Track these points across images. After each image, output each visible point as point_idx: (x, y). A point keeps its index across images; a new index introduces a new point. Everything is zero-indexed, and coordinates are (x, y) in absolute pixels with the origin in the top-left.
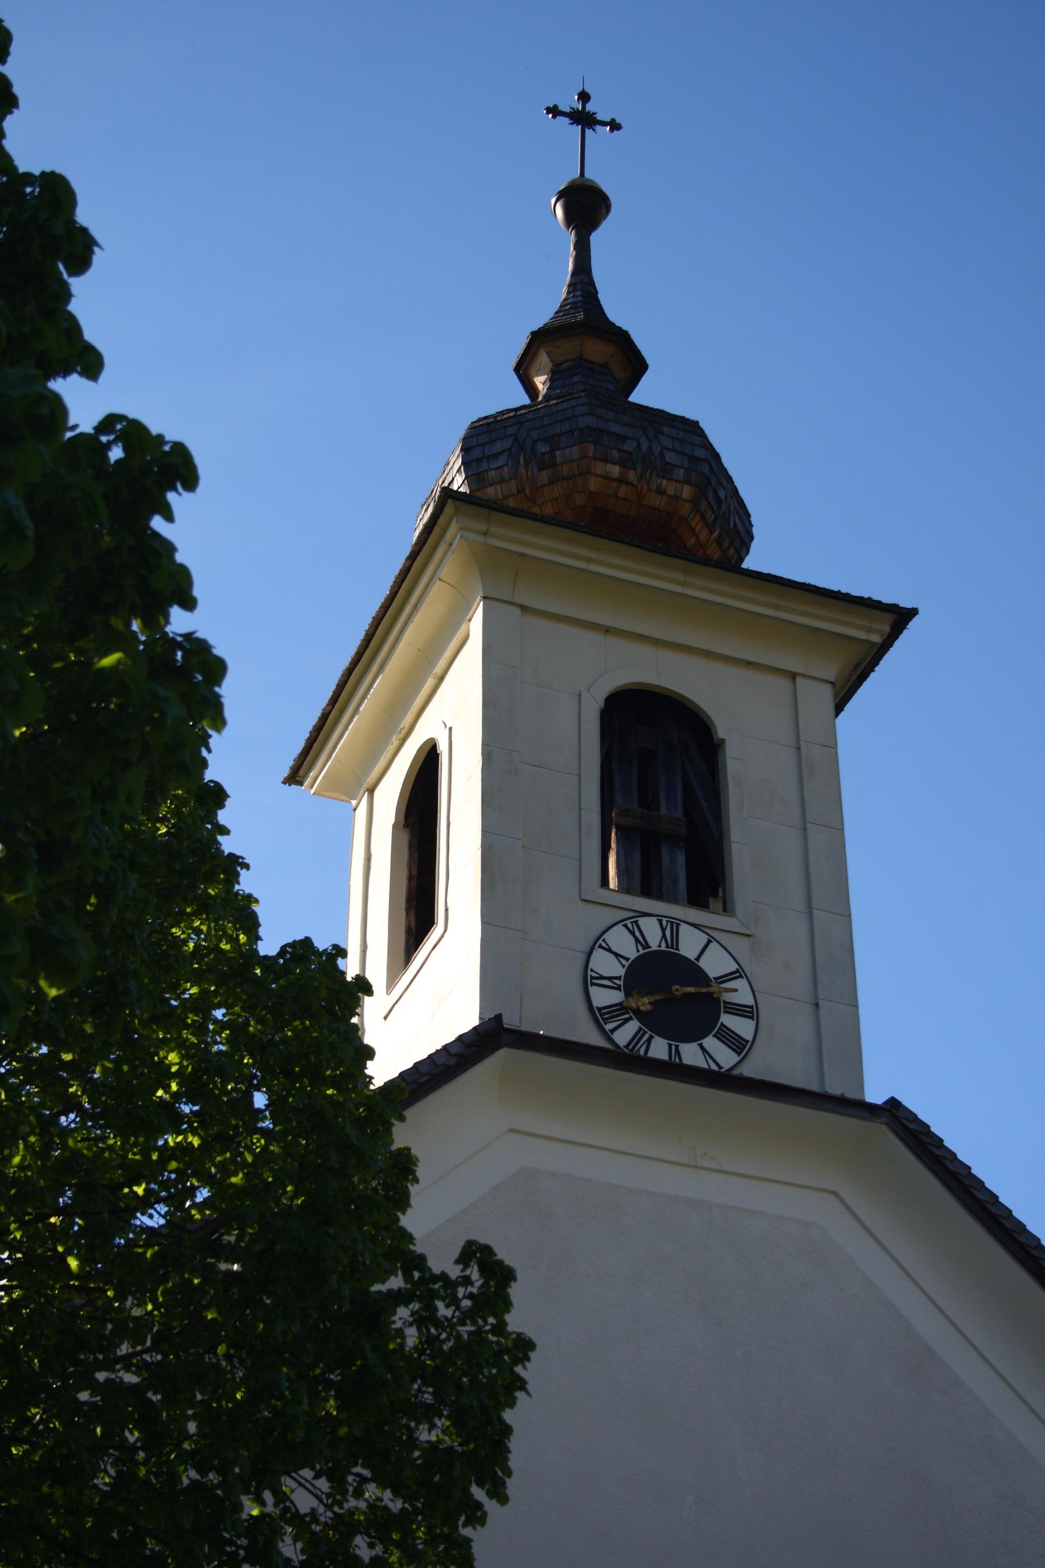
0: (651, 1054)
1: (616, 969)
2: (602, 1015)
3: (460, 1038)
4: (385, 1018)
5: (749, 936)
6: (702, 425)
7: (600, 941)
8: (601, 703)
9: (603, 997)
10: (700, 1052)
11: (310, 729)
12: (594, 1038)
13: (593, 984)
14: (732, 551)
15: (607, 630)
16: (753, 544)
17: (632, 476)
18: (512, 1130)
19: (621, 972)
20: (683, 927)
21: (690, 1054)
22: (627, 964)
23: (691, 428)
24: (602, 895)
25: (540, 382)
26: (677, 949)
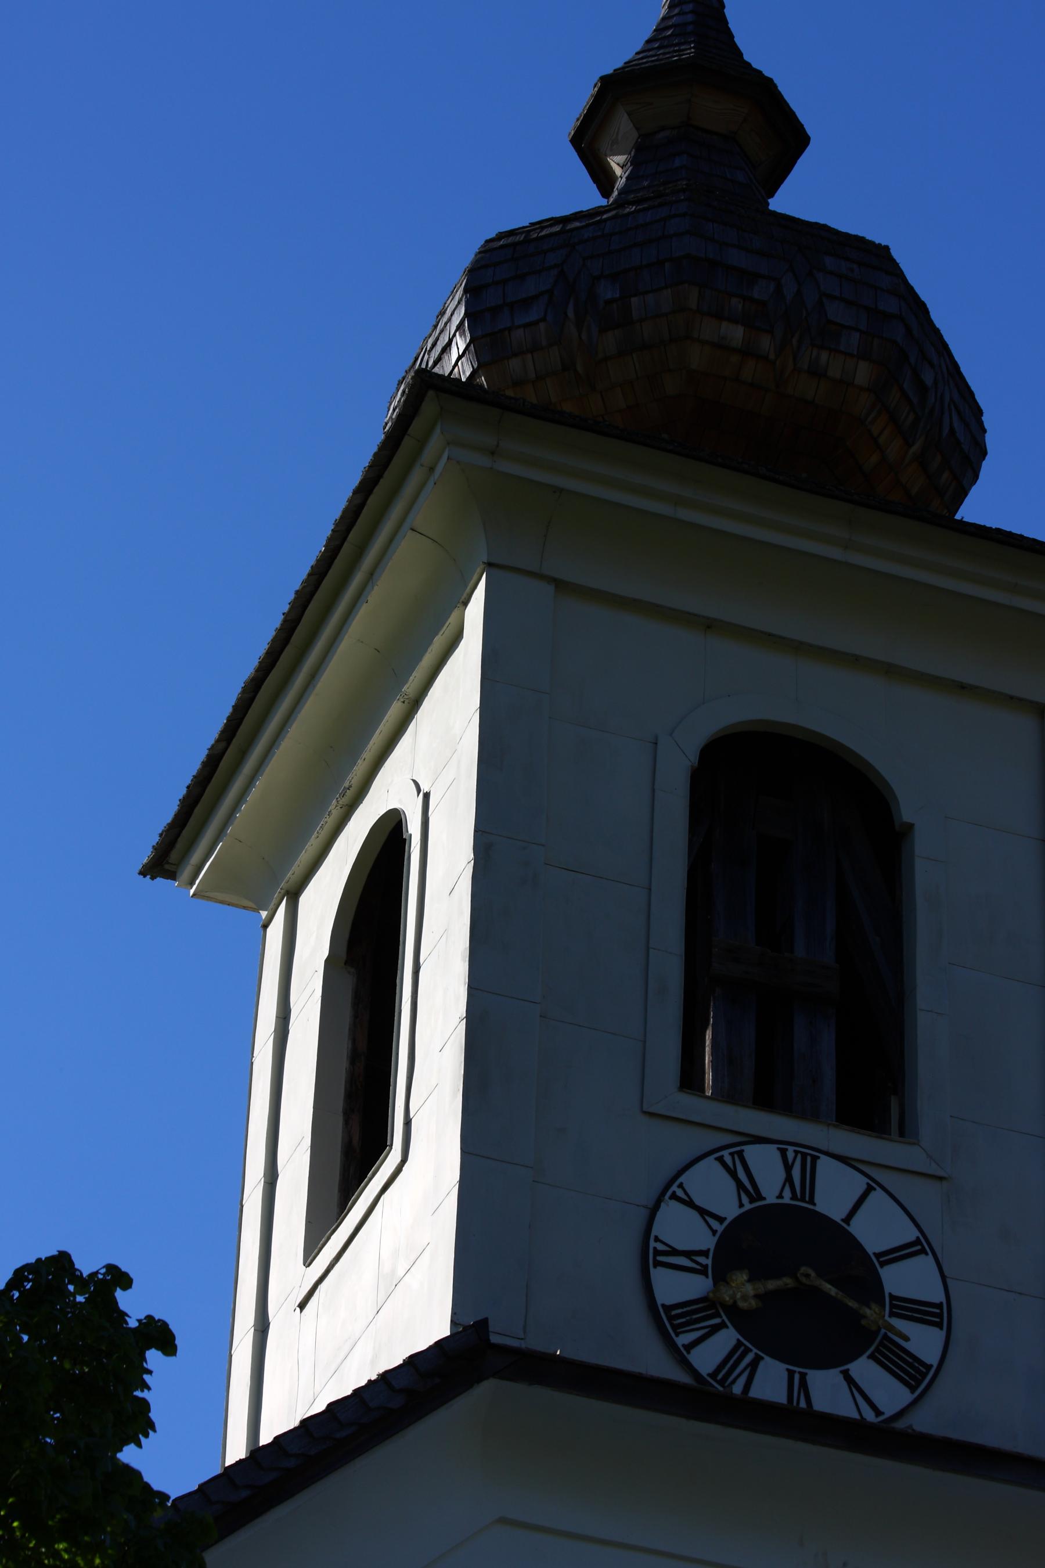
0: (755, 1393)
1: (699, 1237)
2: (671, 1319)
3: (413, 1360)
4: (302, 1306)
5: (941, 1179)
6: (895, 253)
7: (674, 1188)
8: (693, 757)
9: (675, 1287)
10: (844, 1384)
11: (188, 781)
12: (657, 1364)
13: (657, 1264)
14: (946, 475)
15: (710, 625)
16: (985, 464)
17: (766, 343)
18: (503, 1521)
19: (708, 1242)
20: (825, 1165)
21: (828, 1393)
22: (720, 1228)
23: (874, 260)
24: (686, 1103)
25: (617, 164)
26: (812, 1201)
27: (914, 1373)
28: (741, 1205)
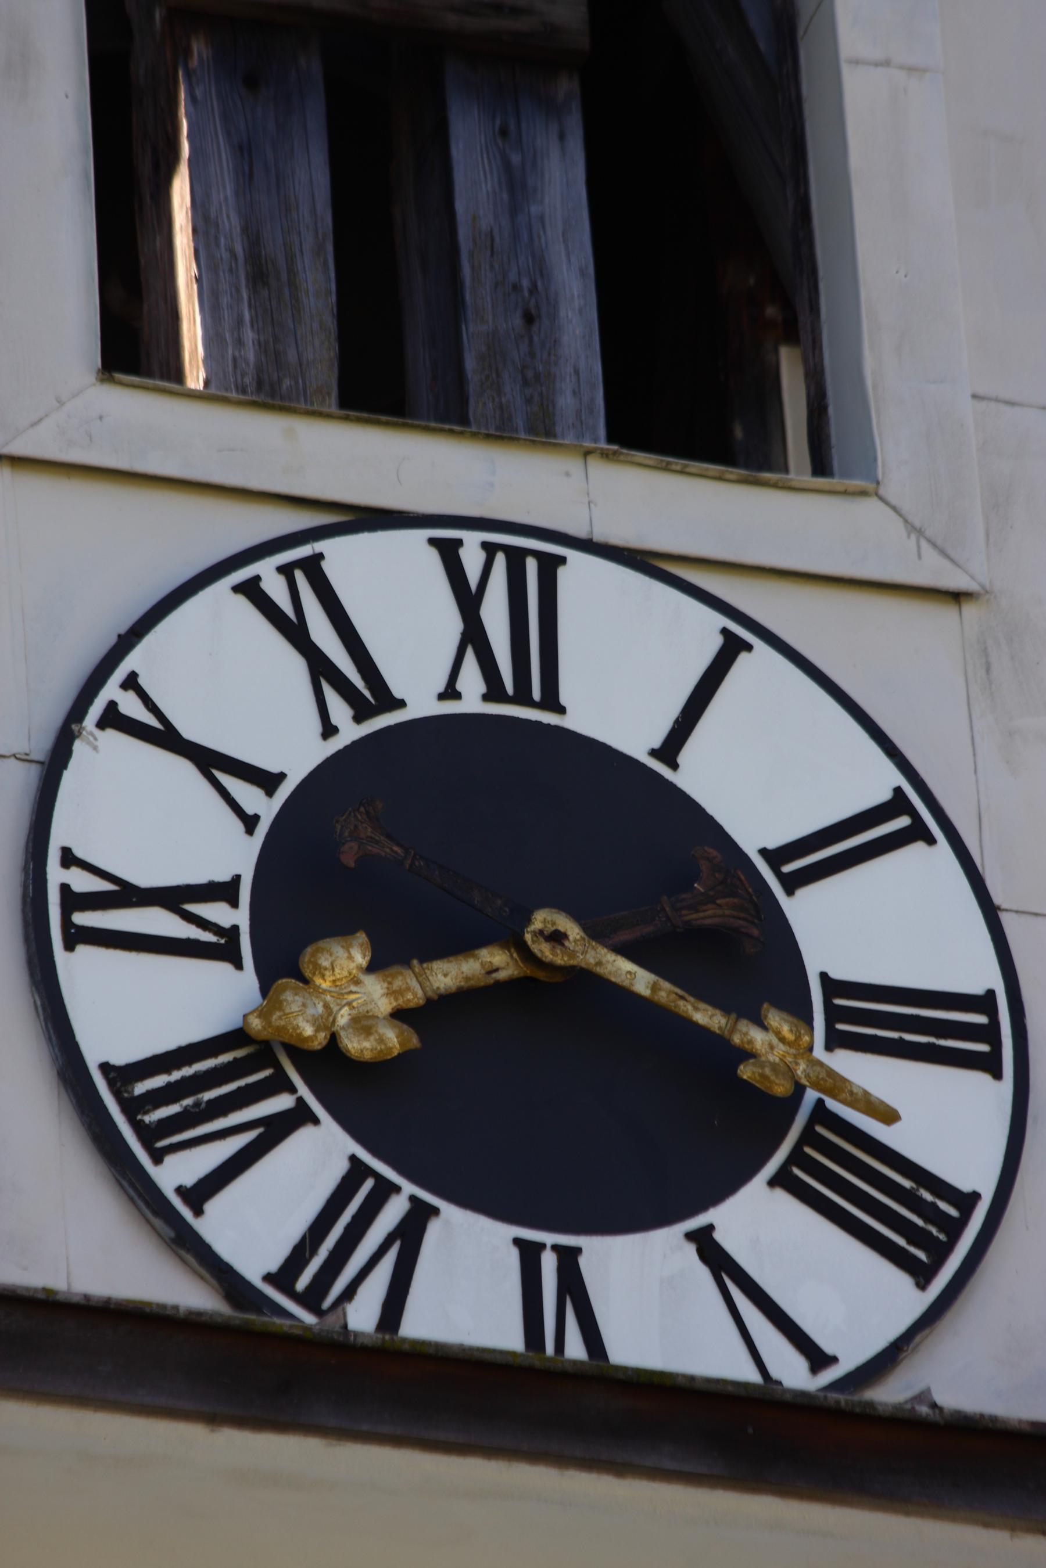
0: (419, 1324)
1: (212, 843)
2: (132, 1107)
5: (957, 597)
7: (111, 691)
9: (140, 1007)
10: (703, 1274)
13: (75, 937)
20: (587, 587)
21: (651, 1303)
24: (133, 420)
26: (552, 702)
27: (921, 1225)
28: (329, 730)
